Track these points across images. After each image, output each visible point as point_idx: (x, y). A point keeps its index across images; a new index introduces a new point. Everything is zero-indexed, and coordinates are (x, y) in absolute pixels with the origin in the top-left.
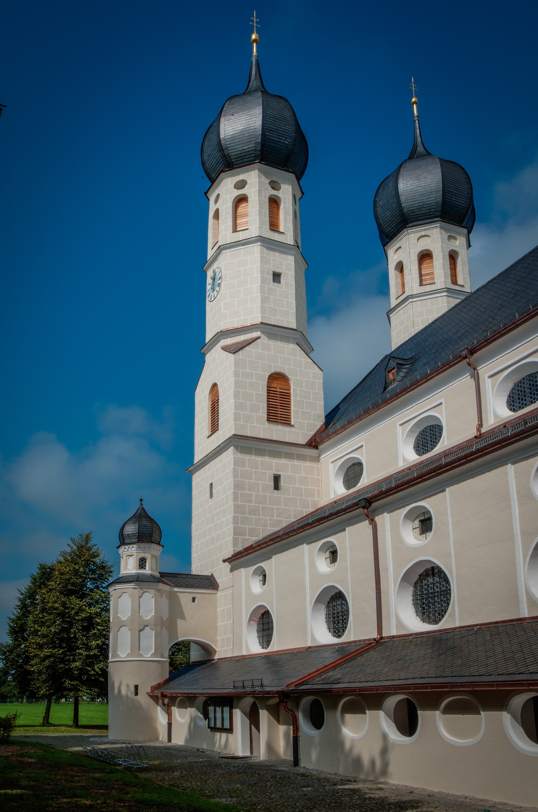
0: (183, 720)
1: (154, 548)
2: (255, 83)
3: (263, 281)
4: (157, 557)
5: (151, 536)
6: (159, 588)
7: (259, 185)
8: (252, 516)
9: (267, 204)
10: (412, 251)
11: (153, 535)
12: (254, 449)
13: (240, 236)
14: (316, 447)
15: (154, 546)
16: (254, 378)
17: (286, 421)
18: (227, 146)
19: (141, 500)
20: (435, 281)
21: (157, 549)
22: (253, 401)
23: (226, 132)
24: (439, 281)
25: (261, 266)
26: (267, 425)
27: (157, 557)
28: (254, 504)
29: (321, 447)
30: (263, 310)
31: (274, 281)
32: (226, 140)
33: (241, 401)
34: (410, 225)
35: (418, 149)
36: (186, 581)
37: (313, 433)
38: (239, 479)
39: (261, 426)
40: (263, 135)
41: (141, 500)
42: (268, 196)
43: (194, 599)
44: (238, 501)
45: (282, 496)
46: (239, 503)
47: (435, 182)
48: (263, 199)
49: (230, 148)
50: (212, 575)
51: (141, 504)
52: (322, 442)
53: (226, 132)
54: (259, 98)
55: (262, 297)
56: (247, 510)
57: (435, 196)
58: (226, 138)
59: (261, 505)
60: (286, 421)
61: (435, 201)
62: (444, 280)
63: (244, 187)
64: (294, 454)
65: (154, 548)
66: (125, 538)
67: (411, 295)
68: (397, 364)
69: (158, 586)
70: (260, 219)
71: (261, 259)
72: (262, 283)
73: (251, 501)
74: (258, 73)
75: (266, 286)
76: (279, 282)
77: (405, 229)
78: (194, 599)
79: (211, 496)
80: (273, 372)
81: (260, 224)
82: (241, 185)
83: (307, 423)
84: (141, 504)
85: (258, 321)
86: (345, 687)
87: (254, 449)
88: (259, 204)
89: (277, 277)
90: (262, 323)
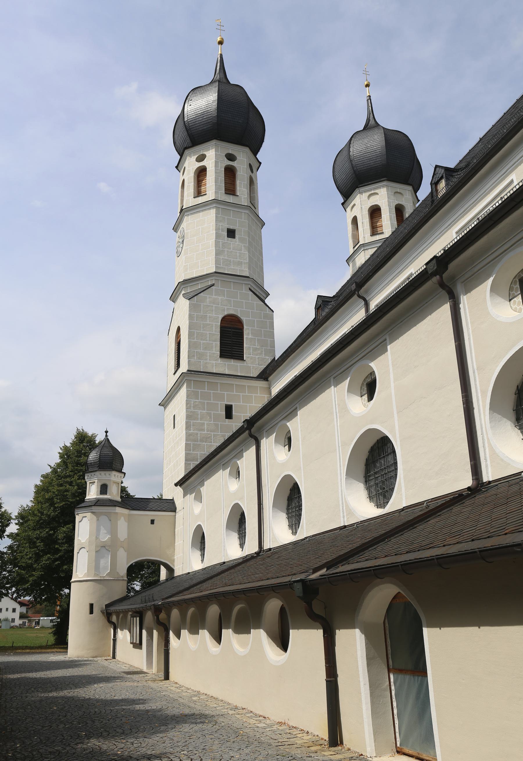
0: (241, 650)
1: (115, 475)
2: (218, 76)
3: (218, 236)
4: (118, 483)
5: (112, 463)
6: (117, 511)
7: (215, 157)
8: (204, 443)
9: (223, 172)
10: (363, 207)
11: (114, 462)
12: (206, 382)
13: (201, 200)
14: (266, 379)
15: (114, 473)
16: (208, 320)
17: (239, 356)
18: (190, 127)
19: (106, 432)
20: (384, 231)
21: (118, 476)
22: (207, 340)
23: (188, 116)
24: (386, 230)
25: (216, 225)
26: (220, 361)
27: (118, 483)
28: (206, 432)
29: (270, 379)
30: (217, 262)
31: (229, 236)
32: (189, 123)
33: (195, 340)
34: (361, 185)
35: (370, 122)
36: (145, 504)
37: (263, 367)
38: (192, 410)
39: (214, 362)
40: (218, 116)
41: (106, 432)
42: (224, 165)
43: (152, 522)
44: (190, 430)
45: (234, 424)
46: (192, 431)
47: (380, 148)
48: (219, 169)
49: (193, 129)
50: (173, 500)
51: (106, 436)
52: (270, 374)
53: (188, 116)
54: (216, 87)
55: (216, 250)
56: (199, 438)
57: (380, 159)
58: (189, 121)
59: (212, 433)
60: (239, 356)
61: (381, 164)
62: (391, 229)
63: (204, 160)
64: (245, 386)
65: (115, 475)
66: (89, 467)
67: (363, 244)
68: (323, 301)
69: (115, 510)
70: (216, 185)
71: (216, 218)
72: (216, 238)
73: (203, 430)
74: (222, 68)
75: (221, 241)
76: (234, 237)
77: (357, 189)
78: (152, 522)
79: (174, 427)
80: (226, 314)
81: (215, 189)
82: (201, 158)
83: (258, 358)
84: (106, 436)
85: (214, 270)
86: (215, 592)
87: (206, 382)
88: (216, 172)
89: (231, 233)
90: (216, 272)
